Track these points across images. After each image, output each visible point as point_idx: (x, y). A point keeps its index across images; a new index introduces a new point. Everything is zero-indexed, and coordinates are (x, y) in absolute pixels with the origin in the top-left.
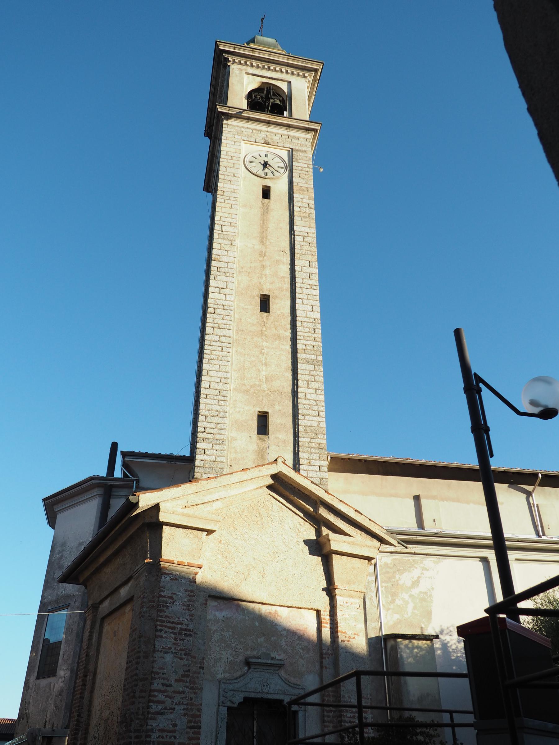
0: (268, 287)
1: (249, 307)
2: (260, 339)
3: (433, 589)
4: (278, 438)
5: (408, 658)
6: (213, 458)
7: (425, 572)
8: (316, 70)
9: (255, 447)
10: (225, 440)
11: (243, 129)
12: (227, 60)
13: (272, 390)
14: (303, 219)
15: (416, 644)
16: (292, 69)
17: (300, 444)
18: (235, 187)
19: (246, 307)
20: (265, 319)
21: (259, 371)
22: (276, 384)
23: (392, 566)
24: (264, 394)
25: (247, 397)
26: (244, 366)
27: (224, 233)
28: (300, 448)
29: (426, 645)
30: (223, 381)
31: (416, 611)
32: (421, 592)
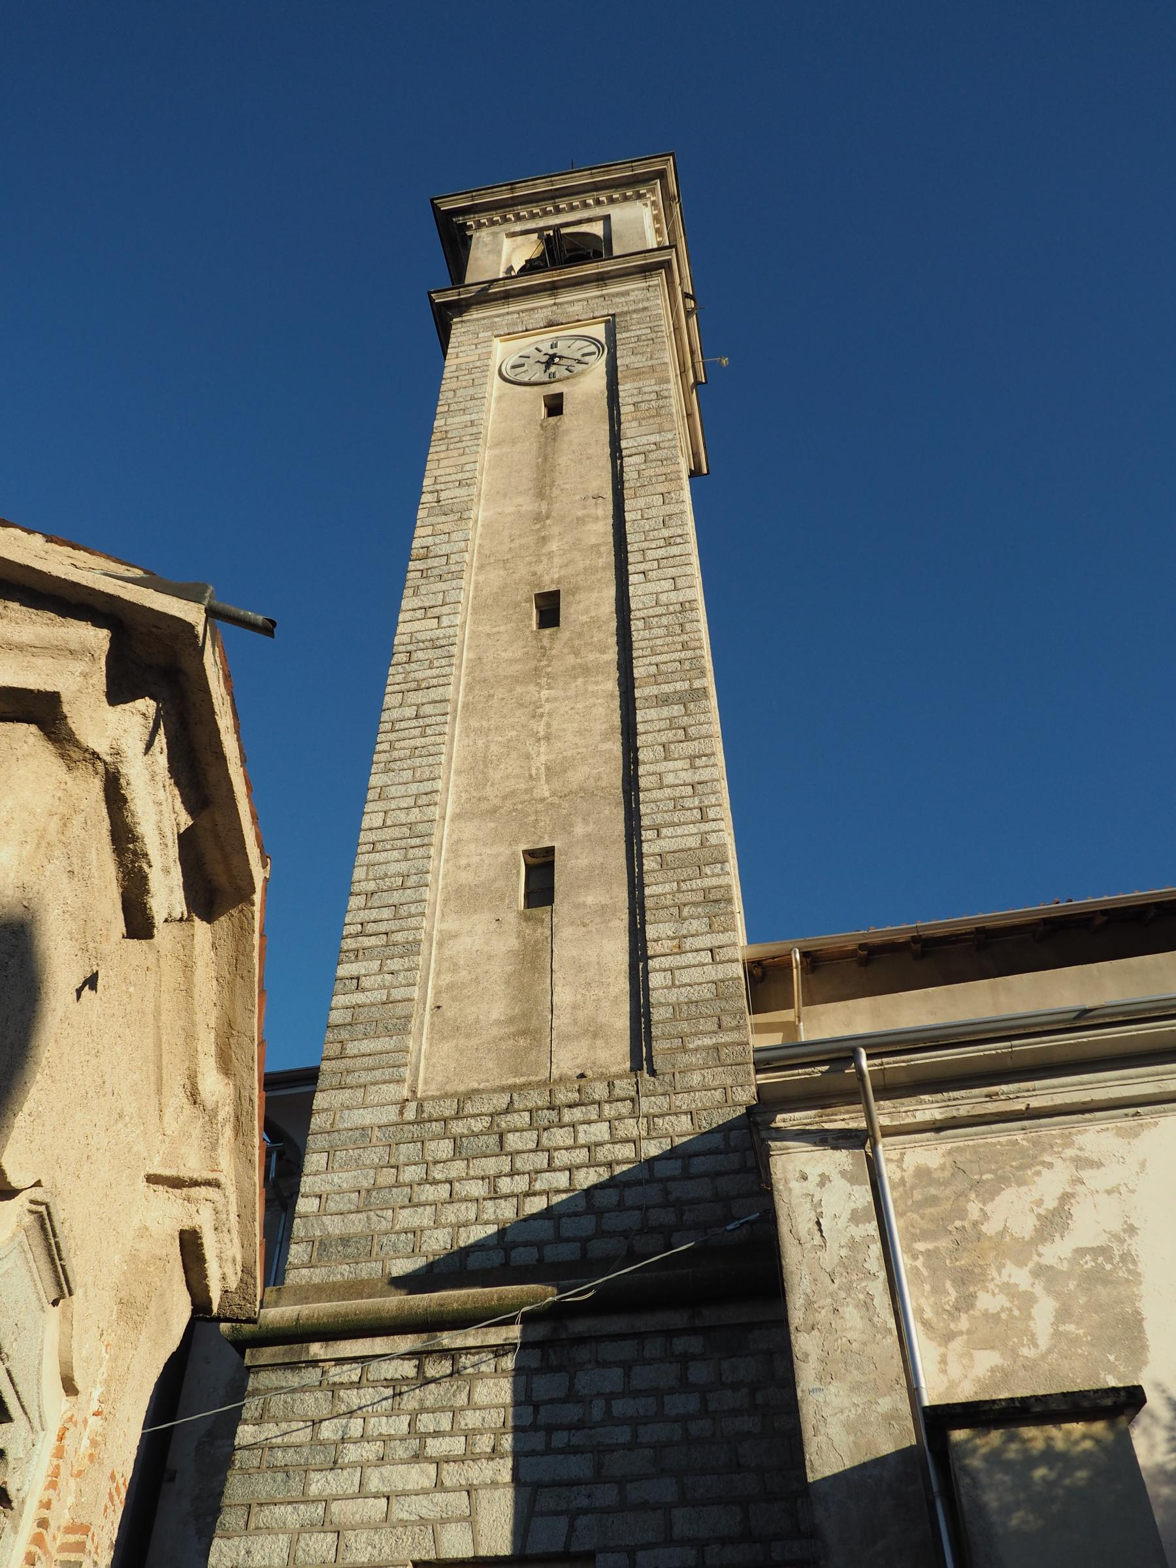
0: (556, 576)
1: (502, 629)
2: (532, 688)
3: (1132, 1230)
4: (584, 904)
5: (1006, 1510)
6: (381, 995)
7: (1085, 1174)
8: (661, 175)
9: (513, 943)
10: (418, 942)
11: (496, 319)
12: (464, 227)
13: (566, 791)
14: (644, 423)
15: (1039, 1445)
16: (608, 192)
17: (649, 903)
18: (474, 417)
19: (495, 630)
20: (546, 642)
21: (528, 757)
22: (577, 776)
23: (947, 1174)
24: (540, 807)
25: (492, 825)
26: (485, 757)
27: (442, 503)
28: (648, 913)
29: (1088, 1444)
30: (423, 800)
31: (1071, 1327)
32: (1081, 1252)
